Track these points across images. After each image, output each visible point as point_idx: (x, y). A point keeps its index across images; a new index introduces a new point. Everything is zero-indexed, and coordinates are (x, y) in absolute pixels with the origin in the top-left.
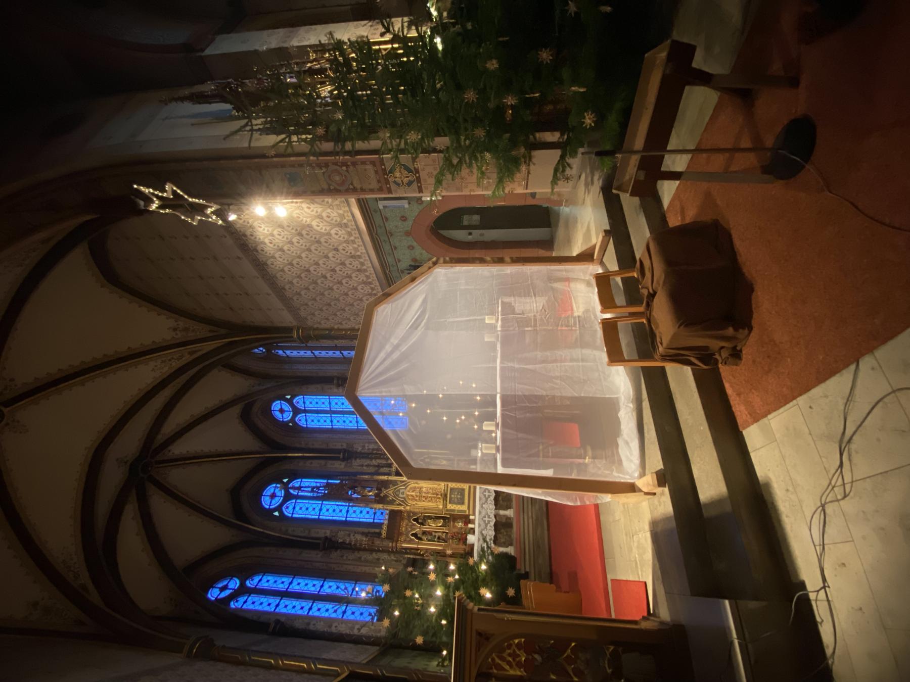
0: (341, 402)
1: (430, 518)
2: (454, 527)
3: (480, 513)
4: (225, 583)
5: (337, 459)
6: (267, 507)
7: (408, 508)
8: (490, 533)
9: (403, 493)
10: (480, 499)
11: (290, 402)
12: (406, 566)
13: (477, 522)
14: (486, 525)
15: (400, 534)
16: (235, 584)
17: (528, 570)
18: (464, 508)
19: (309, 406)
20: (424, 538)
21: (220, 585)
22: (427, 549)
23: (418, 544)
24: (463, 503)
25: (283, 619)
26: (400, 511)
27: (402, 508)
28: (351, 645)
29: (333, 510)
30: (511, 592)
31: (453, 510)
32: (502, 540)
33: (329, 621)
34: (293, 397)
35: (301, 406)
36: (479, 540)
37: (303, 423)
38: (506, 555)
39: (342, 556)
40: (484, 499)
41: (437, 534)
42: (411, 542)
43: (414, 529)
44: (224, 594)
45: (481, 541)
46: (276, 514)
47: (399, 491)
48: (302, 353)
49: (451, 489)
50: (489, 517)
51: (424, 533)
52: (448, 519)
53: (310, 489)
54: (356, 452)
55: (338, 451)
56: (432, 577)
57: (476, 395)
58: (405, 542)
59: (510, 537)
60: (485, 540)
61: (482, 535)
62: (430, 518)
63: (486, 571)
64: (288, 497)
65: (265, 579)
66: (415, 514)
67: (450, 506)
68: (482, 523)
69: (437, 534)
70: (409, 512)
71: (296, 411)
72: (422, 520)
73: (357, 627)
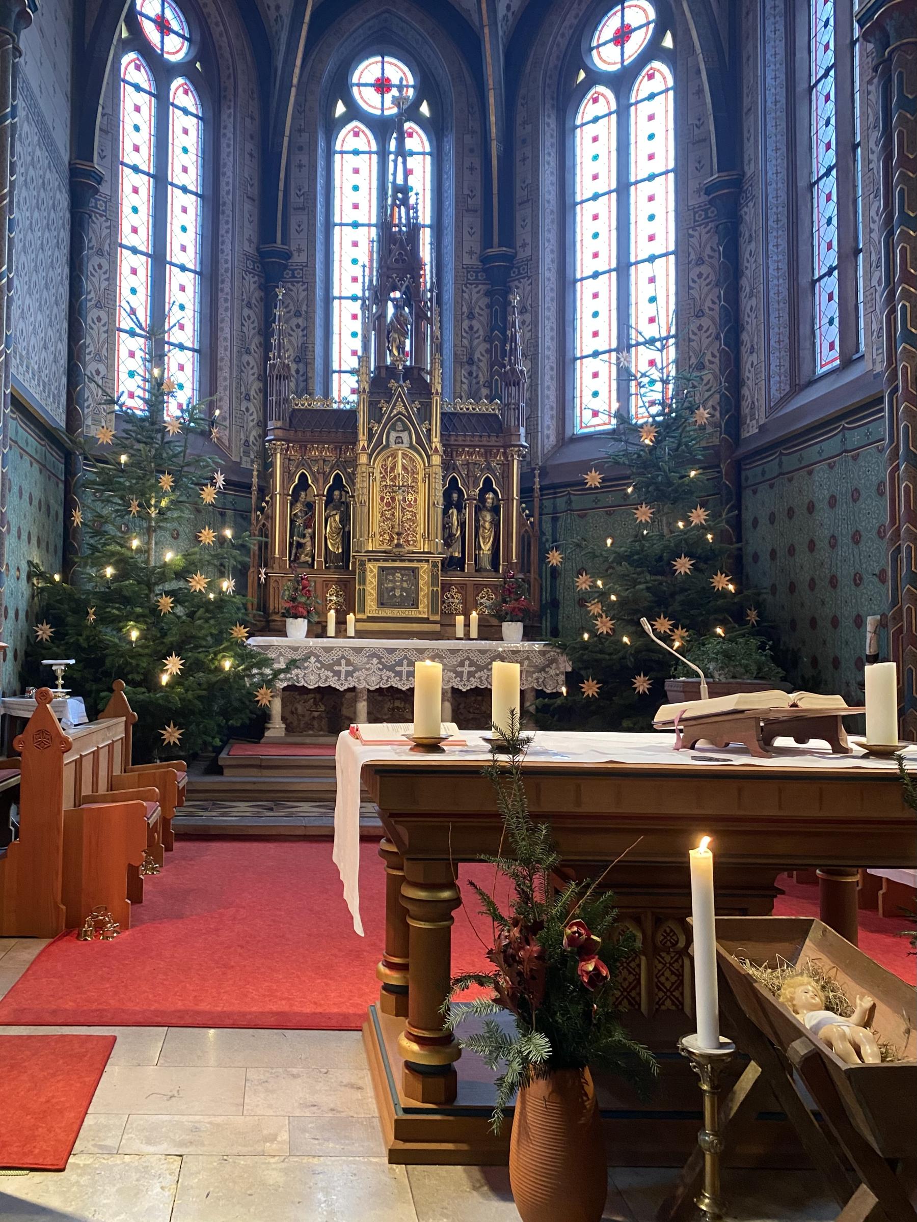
0: (634, 35)
1: (345, 520)
2: (327, 584)
3: (358, 650)
4: (175, 25)
5: (487, 242)
6: (355, 79)
7: (363, 459)
8: (311, 677)
9: (399, 441)
10: (391, 651)
11: (652, 51)
12: (232, 469)
13: (341, 642)
14: (329, 668)
15: (303, 447)
16: (175, 49)
17: (226, 771)
18: (372, 607)
19: (639, 114)
20: (298, 508)
21: (169, 14)
22: (273, 518)
23: (284, 495)
24: (381, 604)
25: (104, 189)
26: (355, 442)
27: (363, 442)
28: (63, 361)
29: (352, 258)
30: (172, 734)
31: (363, 581)
32: (300, 708)
33: (108, 300)
34: (669, 57)
35: (643, 87)
36: (295, 649)
37: (588, 110)
38: (264, 716)
39: (249, 305)
40: (391, 660)
41: (307, 541)
42: (288, 474)
43: (316, 480)
44: (151, 31)
45: (291, 655)
46: (340, 109)
47: (406, 429)
48: (827, 36)
49: (415, 571)
50: (349, 674)
51: (310, 506)
52: (344, 563)
53: (400, 181)
54: (507, 291)
55: (508, 237)
56: (207, 536)
57: (586, 467)
58: (287, 460)
59: (309, 726)
60: (292, 664)
61: (306, 659)
62: (345, 520)
63: (219, 669)
64: (382, 128)
65: (191, 123)
66: (352, 478)
67: (372, 569)
68: (396, 657)
69: (307, 541)
70: (353, 462)
71: (622, 82)
72: (340, 497)
73: (102, 368)
